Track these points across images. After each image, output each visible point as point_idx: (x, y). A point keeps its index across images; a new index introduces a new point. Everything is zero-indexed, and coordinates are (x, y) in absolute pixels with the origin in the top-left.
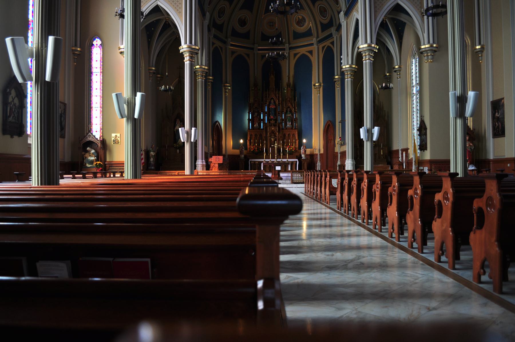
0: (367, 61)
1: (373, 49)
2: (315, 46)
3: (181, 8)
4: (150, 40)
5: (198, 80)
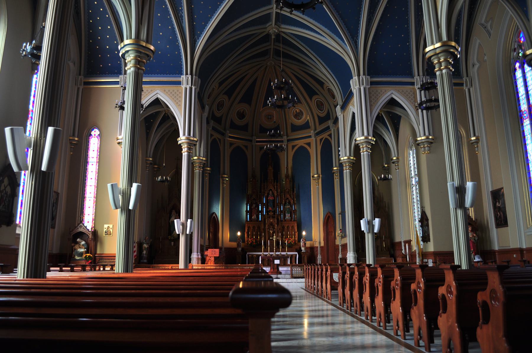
0: (365, 153)
1: (370, 142)
2: (313, 138)
3: (180, 101)
4: (148, 131)
5: (195, 171)
